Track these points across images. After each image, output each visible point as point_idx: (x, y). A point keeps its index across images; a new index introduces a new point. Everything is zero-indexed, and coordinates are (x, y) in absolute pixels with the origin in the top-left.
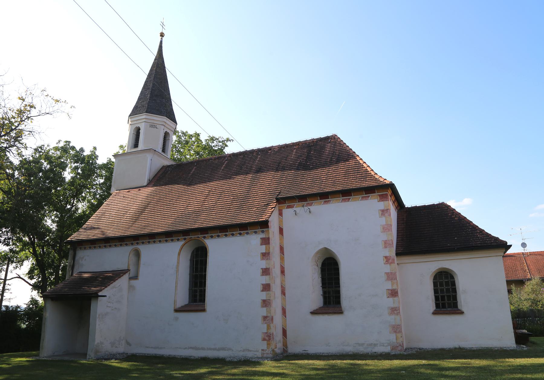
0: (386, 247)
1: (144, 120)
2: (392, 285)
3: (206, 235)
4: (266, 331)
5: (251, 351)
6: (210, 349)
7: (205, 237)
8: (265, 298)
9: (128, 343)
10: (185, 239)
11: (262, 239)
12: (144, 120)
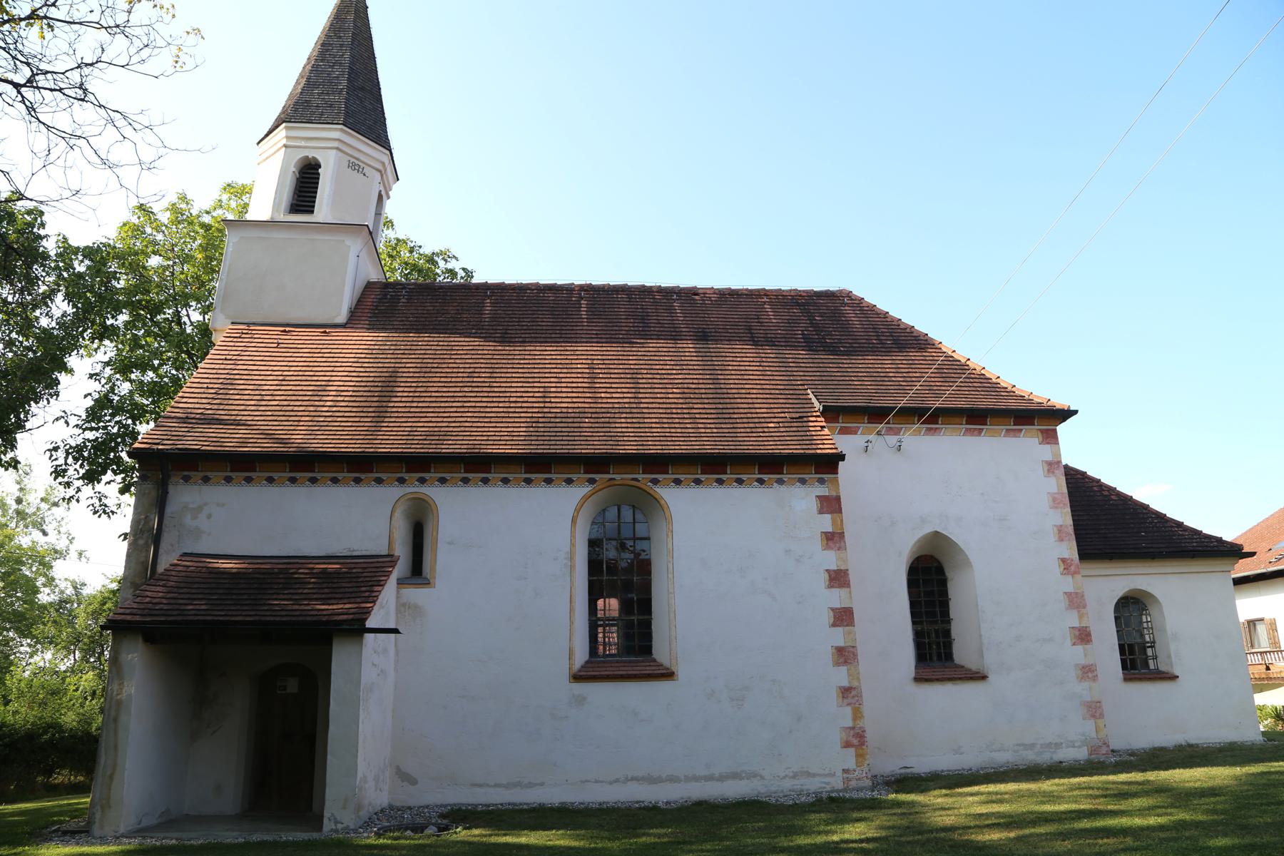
0: (1061, 540)
1: (336, 144)
2: (1081, 617)
4: (851, 724)
5: (814, 775)
6: (696, 779)
7: (655, 482)
8: (842, 644)
9: (405, 777)
10: (592, 481)
11: (821, 498)
12: (336, 144)
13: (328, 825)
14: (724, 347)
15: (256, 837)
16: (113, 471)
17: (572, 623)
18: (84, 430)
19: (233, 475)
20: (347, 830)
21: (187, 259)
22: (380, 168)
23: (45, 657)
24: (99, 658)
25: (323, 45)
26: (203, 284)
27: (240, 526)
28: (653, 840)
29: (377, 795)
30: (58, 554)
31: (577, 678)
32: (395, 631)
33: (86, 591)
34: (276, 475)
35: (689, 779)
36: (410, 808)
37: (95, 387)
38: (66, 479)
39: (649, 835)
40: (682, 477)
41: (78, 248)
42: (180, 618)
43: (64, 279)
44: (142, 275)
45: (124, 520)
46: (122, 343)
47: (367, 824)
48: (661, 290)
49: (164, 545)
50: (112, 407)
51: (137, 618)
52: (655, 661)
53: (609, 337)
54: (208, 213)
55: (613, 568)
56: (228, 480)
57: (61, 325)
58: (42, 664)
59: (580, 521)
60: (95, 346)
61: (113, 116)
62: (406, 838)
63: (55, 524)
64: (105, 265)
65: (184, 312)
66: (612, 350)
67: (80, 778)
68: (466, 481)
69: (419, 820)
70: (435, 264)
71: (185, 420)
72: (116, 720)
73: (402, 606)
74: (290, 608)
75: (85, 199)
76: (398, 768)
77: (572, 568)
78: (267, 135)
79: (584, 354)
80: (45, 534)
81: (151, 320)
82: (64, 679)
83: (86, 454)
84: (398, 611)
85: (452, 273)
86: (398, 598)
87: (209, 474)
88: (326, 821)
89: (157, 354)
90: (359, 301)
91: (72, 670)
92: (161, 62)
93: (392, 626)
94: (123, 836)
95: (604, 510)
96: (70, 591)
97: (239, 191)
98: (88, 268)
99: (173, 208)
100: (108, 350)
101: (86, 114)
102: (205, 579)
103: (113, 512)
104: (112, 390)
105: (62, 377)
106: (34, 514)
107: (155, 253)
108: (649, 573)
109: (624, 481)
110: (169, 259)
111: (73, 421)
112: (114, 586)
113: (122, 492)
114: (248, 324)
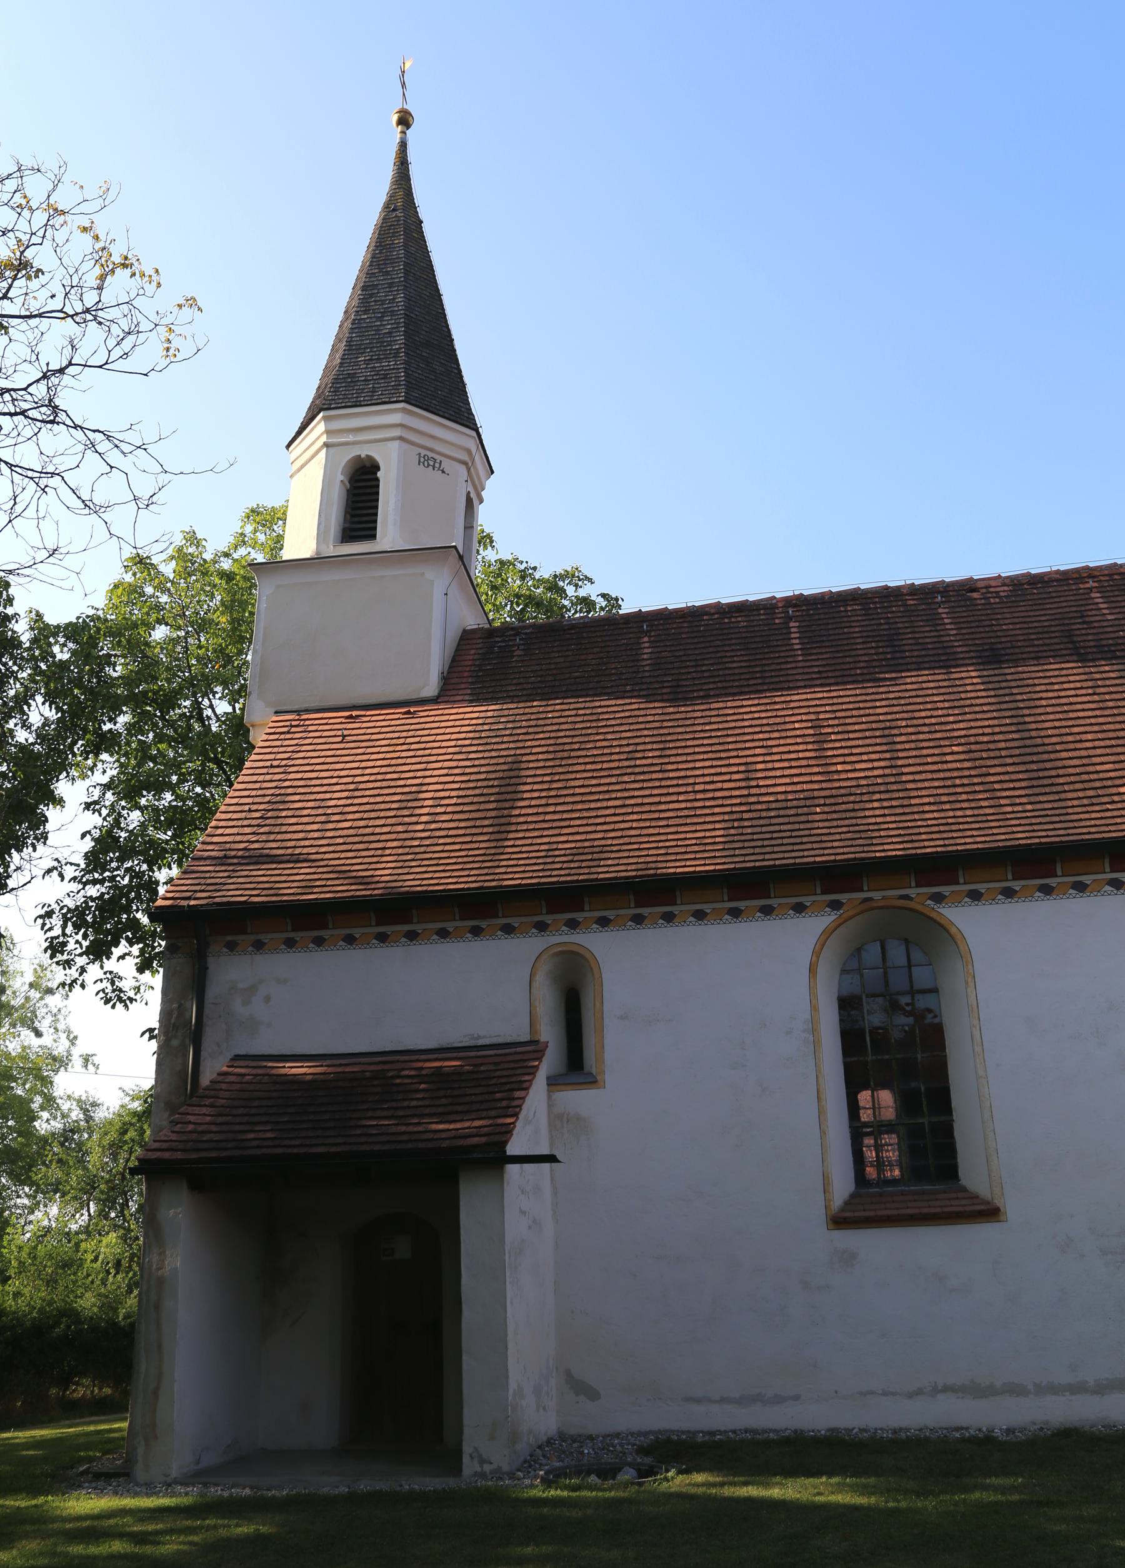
1: (397, 432)
3: (945, 890)
6: (1054, 1389)
7: (938, 898)
10: (835, 905)
12: (397, 432)
13: (469, 1467)
14: (1029, 670)
15: (365, 1486)
16: (128, 939)
17: (823, 1133)
18: (85, 884)
19: (297, 936)
20: (498, 1474)
21: (203, 625)
22: (466, 458)
23: (50, 1213)
24: (122, 1212)
25: (364, 288)
26: (229, 660)
27: (318, 1009)
28: (992, 1497)
29: (539, 1414)
30: (60, 1062)
31: (840, 1221)
32: (551, 1159)
33: (100, 1115)
34: (357, 932)
35: (1042, 1390)
36: (590, 1438)
37: (92, 821)
38: (65, 957)
39: (985, 1488)
40: (982, 887)
41: (58, 627)
42: (237, 1153)
43: (41, 673)
44: (145, 656)
45: (149, 1010)
46: (126, 755)
47: (529, 1464)
48: (914, 591)
49: (208, 1045)
50: (120, 848)
51: (179, 1155)
52: (964, 1189)
53: (839, 674)
54: (226, 555)
55: (880, 1038)
56: (290, 944)
57: (41, 736)
58: (46, 1223)
59: (822, 970)
60: (90, 762)
61: (95, 439)
62: (591, 1488)
63: (49, 1019)
64: (95, 646)
65: (206, 702)
66: (848, 694)
67: (107, 1391)
68: (638, 920)
69: (607, 1458)
70: (562, 592)
71: (222, 860)
72: (157, 1307)
73: (558, 1120)
74: (393, 1129)
75: (68, 561)
76: (569, 1374)
77: (816, 1044)
78: (299, 433)
79: (802, 706)
80: (38, 1034)
81: (162, 718)
82: (77, 1245)
83: (89, 918)
84: (552, 1127)
85: (587, 603)
86: (550, 1106)
87: (261, 937)
88: (466, 1459)
89: (175, 766)
90: (453, 660)
91: (86, 1230)
92: (149, 351)
93: (545, 1151)
94: (176, 1482)
95: (859, 950)
96: (76, 1114)
97: (268, 519)
98: (74, 653)
99: (180, 555)
100: (107, 767)
101: (55, 439)
102: (265, 1091)
103: (131, 1000)
104: (117, 823)
105: (52, 813)
106: (23, 1006)
107: (159, 622)
108: (943, 1048)
109: (889, 909)
110: (179, 628)
111: (69, 872)
112: (137, 1105)
113: (141, 969)
114: (298, 712)
